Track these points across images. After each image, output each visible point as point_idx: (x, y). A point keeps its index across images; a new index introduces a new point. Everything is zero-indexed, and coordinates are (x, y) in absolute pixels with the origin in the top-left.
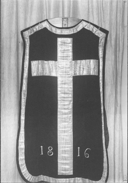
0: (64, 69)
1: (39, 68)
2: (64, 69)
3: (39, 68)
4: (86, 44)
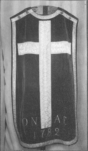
4: (62, 28)
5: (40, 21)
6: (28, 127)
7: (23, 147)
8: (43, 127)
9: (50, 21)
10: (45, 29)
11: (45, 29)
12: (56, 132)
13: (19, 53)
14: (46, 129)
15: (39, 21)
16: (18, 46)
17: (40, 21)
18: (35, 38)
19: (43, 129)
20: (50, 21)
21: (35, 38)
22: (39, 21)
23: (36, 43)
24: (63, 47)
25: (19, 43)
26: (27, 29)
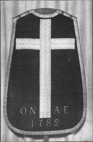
0: (45, 44)
1: (24, 44)
2: (45, 44)
3: (24, 44)
4: (63, 26)
5: (41, 20)
6: (21, 111)
7: (6, 57)
8: (41, 117)
9: (51, 20)
10: (45, 27)
11: (45, 27)
12: (55, 123)
13: (16, 47)
14: (45, 119)
15: (41, 20)
16: (16, 40)
17: (41, 20)
18: (35, 35)
19: (41, 119)
20: (51, 20)
21: (35, 35)
22: (41, 20)
23: (40, 51)
24: (65, 44)
25: (17, 38)
26: (27, 26)
